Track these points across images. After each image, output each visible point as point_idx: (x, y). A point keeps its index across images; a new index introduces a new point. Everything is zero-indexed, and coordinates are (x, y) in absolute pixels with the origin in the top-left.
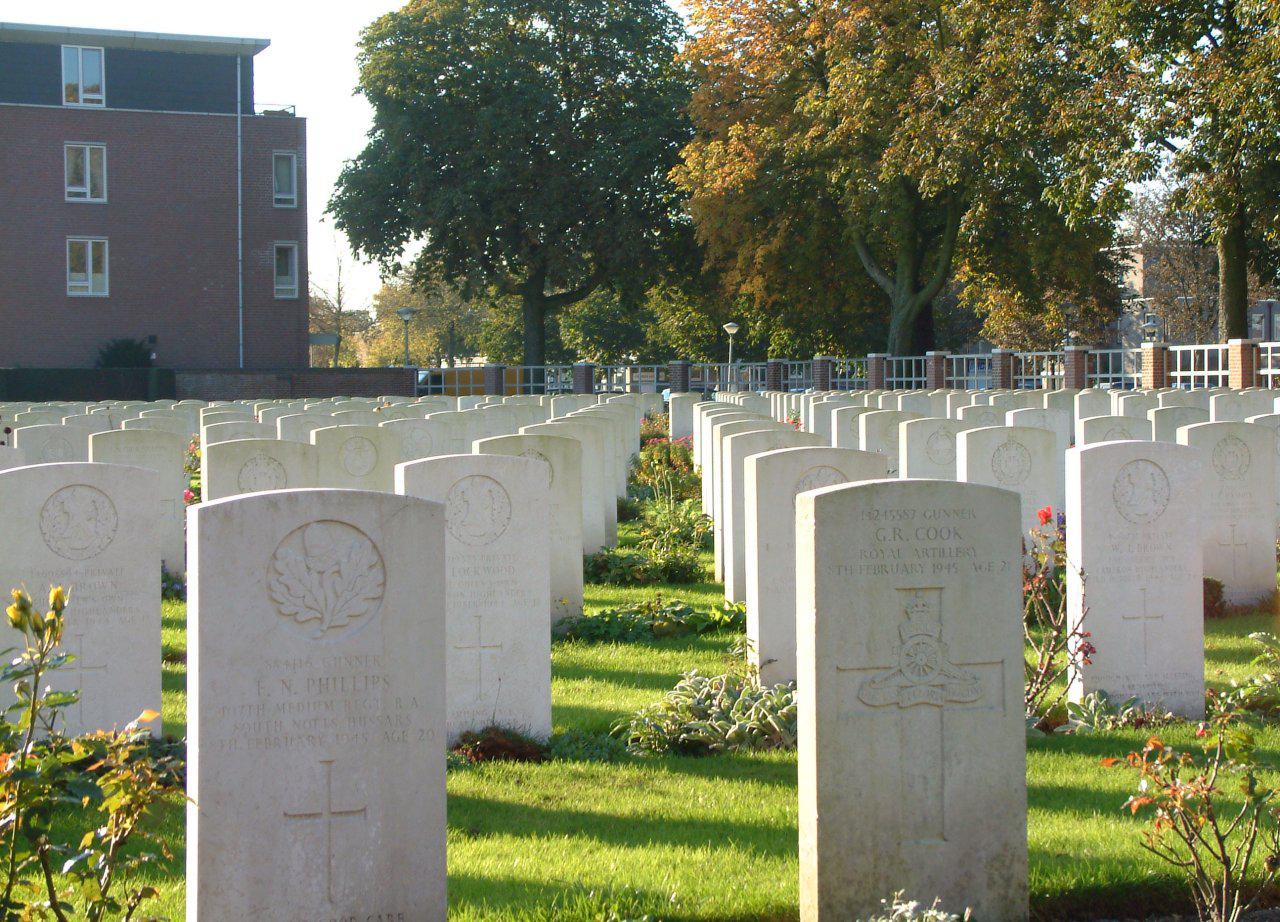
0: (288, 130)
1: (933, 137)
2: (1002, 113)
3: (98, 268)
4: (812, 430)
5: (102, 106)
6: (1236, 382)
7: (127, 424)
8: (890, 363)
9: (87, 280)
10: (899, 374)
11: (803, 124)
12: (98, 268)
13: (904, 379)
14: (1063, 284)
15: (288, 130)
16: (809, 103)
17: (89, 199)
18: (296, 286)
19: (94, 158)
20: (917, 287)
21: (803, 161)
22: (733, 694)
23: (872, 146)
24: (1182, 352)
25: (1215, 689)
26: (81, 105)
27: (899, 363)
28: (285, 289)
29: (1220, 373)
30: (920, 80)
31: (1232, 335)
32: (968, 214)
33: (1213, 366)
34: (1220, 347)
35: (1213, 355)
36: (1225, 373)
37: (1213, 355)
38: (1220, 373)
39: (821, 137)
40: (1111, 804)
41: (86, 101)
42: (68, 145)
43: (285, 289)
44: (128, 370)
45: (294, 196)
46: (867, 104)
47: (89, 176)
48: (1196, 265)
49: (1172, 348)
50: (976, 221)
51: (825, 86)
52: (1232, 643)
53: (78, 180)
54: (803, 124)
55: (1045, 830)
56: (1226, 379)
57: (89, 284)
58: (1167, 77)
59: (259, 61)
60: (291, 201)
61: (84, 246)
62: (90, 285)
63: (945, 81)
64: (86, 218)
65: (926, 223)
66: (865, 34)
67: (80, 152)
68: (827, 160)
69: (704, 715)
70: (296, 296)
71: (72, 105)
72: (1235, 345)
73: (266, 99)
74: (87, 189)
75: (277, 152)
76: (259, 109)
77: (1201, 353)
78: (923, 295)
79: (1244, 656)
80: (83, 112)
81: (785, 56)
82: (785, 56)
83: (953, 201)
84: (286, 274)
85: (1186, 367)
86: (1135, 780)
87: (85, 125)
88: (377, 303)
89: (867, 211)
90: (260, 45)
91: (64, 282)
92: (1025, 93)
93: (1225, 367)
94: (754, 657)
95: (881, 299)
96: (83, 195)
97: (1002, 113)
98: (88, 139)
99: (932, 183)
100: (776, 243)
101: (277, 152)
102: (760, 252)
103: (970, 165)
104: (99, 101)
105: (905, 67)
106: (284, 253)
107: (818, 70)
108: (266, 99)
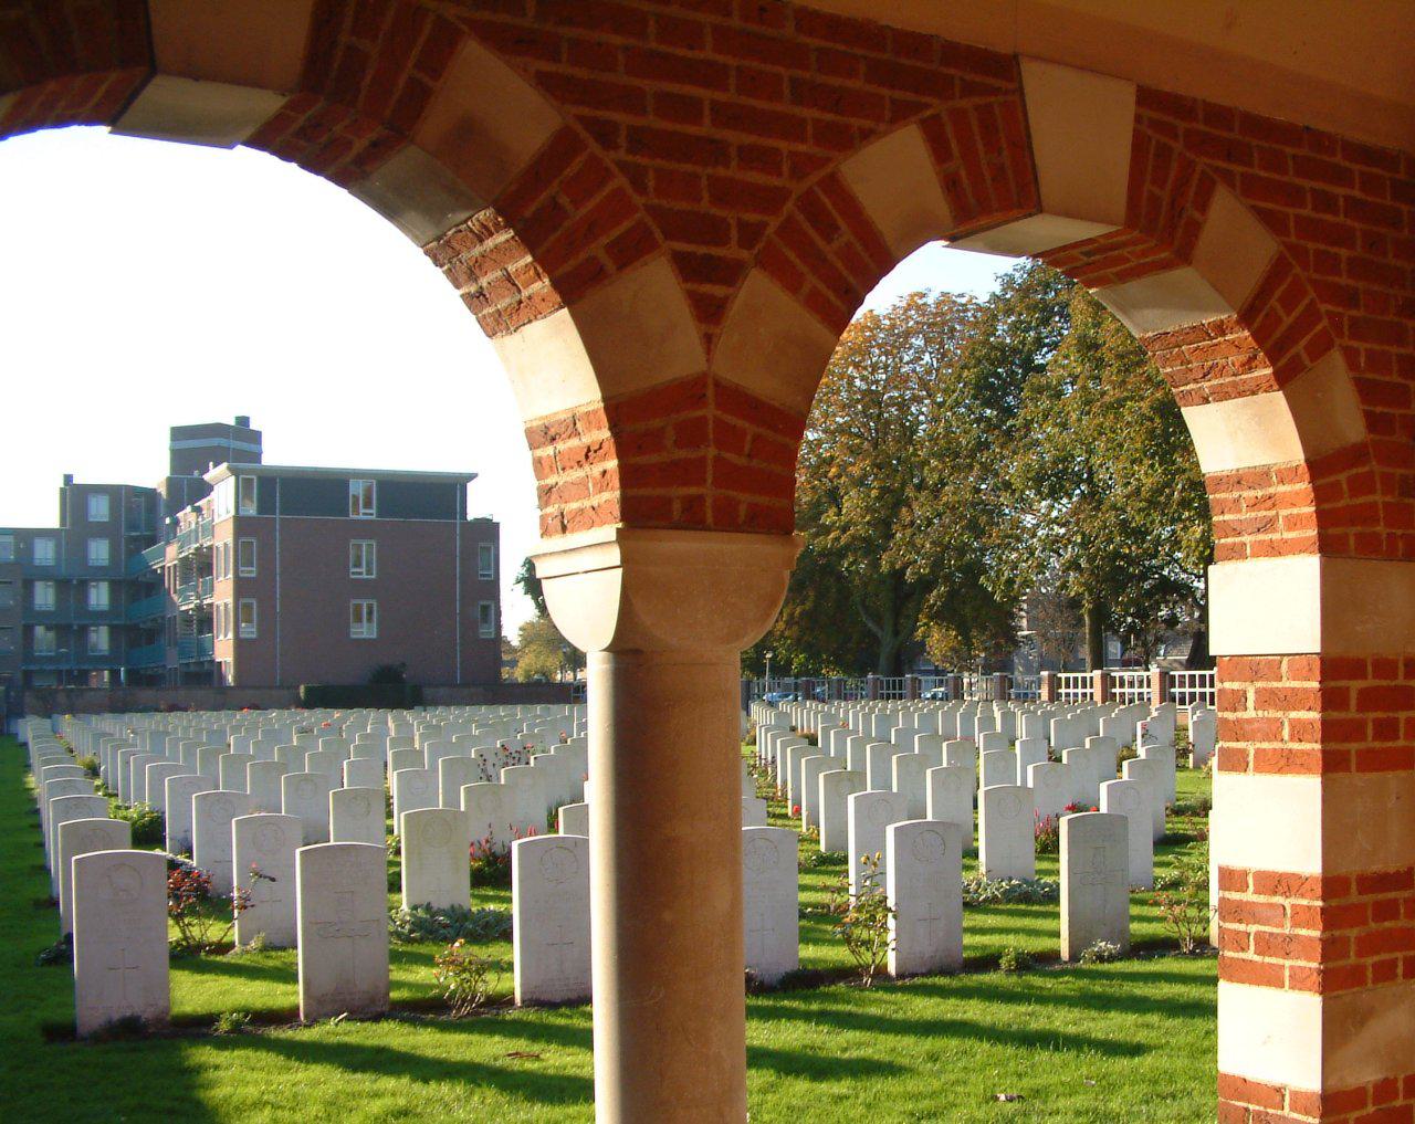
0: (488, 531)
1: (914, 545)
2: (956, 531)
3: (370, 620)
4: (1030, 784)
5: (374, 517)
6: (1098, 697)
7: (549, 751)
8: (882, 682)
9: (362, 627)
10: (888, 688)
11: (827, 530)
12: (370, 620)
13: (891, 692)
14: (983, 629)
15: (488, 531)
16: (829, 518)
17: (365, 577)
18: (492, 630)
19: (367, 549)
20: (896, 633)
21: (825, 553)
22: (979, 885)
23: (871, 548)
24: (1200, 676)
25: (1156, 879)
26: (361, 517)
27: (888, 682)
28: (486, 632)
29: (1088, 691)
30: (904, 510)
31: (1095, 667)
32: (935, 592)
33: (1084, 686)
34: (1088, 675)
35: (1084, 679)
36: (1092, 691)
37: (1084, 679)
38: (1088, 691)
39: (837, 539)
40: (1149, 920)
41: (364, 514)
42: (353, 541)
43: (486, 632)
44: (390, 688)
45: (492, 572)
46: (868, 518)
47: (365, 562)
48: (1062, 611)
49: (1059, 675)
50: (939, 596)
51: (840, 510)
52: (1164, 858)
53: (358, 565)
54: (827, 530)
55: (1135, 927)
56: (1092, 694)
57: (365, 630)
58: (1054, 514)
59: (471, 486)
60: (489, 575)
61: (360, 606)
62: (365, 631)
63: (920, 511)
64: (363, 588)
65: (903, 595)
66: (865, 476)
67: (359, 547)
68: (841, 554)
69: (968, 892)
70: (493, 636)
71: (355, 517)
72: (1097, 674)
73: (474, 511)
74: (364, 570)
75: (482, 544)
76: (470, 517)
77: (1076, 679)
78: (900, 638)
79: (1168, 864)
80: (362, 521)
81: (813, 488)
82: (813, 488)
83: (926, 585)
84: (486, 622)
85: (1122, 686)
86: (1156, 912)
87: (365, 530)
88: (521, 633)
89: (865, 585)
90: (472, 477)
91: (348, 627)
92: (970, 521)
93: (1091, 687)
94: (983, 869)
95: (876, 640)
96: (360, 573)
97: (956, 531)
98: (363, 538)
99: (913, 574)
100: (808, 605)
101: (482, 544)
102: (798, 610)
103: (937, 564)
104: (372, 514)
105: (894, 501)
106: (485, 609)
107: (834, 497)
108: (474, 511)
